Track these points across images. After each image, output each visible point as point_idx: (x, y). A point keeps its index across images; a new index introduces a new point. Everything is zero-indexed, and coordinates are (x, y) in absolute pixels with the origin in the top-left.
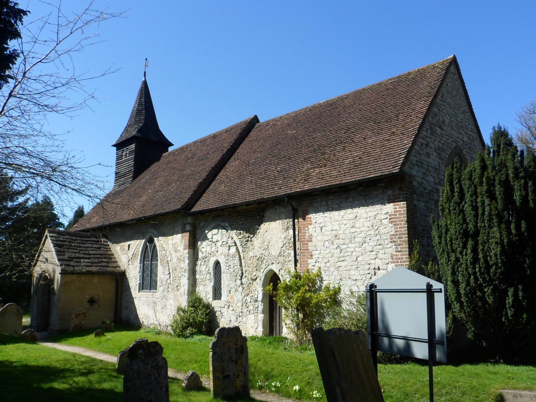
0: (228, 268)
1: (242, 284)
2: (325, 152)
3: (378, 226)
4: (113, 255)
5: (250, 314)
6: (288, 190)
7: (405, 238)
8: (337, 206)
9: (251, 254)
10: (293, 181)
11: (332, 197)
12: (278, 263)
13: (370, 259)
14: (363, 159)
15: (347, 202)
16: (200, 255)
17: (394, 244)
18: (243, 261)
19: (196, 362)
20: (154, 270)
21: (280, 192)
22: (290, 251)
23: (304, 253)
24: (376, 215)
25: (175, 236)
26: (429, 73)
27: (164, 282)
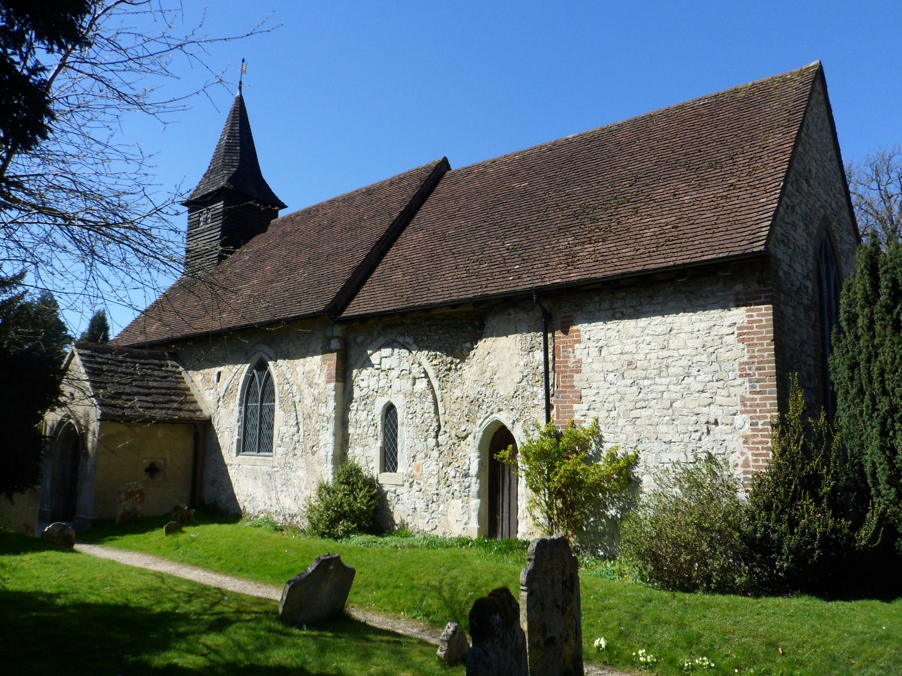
0: (410, 416)
1: (438, 445)
2: (599, 217)
3: (716, 348)
4: (188, 389)
5: (453, 498)
6: (536, 281)
7: (770, 368)
8: (632, 310)
9: (457, 393)
10: (543, 265)
11: (623, 294)
12: (512, 409)
13: (699, 406)
14: (681, 228)
15: (654, 304)
16: (357, 393)
17: (747, 379)
18: (440, 404)
19: (378, 587)
20: (267, 417)
21: (520, 284)
22: (535, 389)
23: (565, 392)
24: (710, 328)
25: (309, 359)
26: (776, 89)
27: (287, 439)
